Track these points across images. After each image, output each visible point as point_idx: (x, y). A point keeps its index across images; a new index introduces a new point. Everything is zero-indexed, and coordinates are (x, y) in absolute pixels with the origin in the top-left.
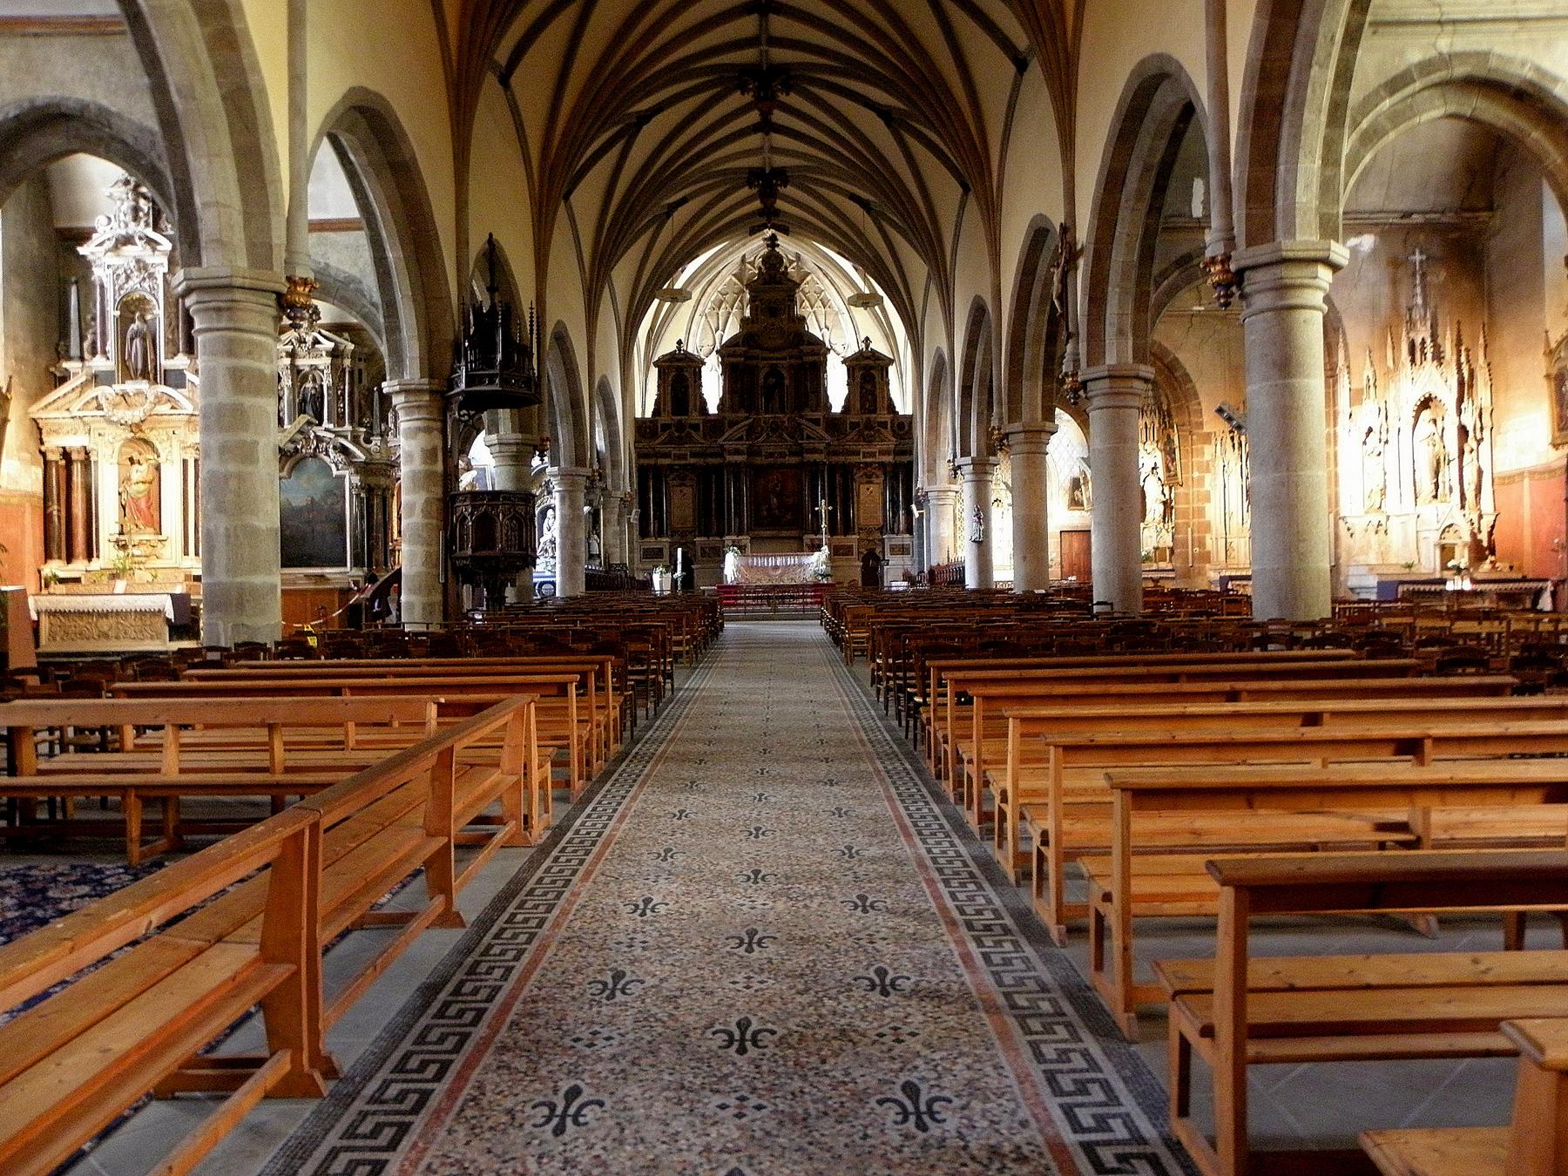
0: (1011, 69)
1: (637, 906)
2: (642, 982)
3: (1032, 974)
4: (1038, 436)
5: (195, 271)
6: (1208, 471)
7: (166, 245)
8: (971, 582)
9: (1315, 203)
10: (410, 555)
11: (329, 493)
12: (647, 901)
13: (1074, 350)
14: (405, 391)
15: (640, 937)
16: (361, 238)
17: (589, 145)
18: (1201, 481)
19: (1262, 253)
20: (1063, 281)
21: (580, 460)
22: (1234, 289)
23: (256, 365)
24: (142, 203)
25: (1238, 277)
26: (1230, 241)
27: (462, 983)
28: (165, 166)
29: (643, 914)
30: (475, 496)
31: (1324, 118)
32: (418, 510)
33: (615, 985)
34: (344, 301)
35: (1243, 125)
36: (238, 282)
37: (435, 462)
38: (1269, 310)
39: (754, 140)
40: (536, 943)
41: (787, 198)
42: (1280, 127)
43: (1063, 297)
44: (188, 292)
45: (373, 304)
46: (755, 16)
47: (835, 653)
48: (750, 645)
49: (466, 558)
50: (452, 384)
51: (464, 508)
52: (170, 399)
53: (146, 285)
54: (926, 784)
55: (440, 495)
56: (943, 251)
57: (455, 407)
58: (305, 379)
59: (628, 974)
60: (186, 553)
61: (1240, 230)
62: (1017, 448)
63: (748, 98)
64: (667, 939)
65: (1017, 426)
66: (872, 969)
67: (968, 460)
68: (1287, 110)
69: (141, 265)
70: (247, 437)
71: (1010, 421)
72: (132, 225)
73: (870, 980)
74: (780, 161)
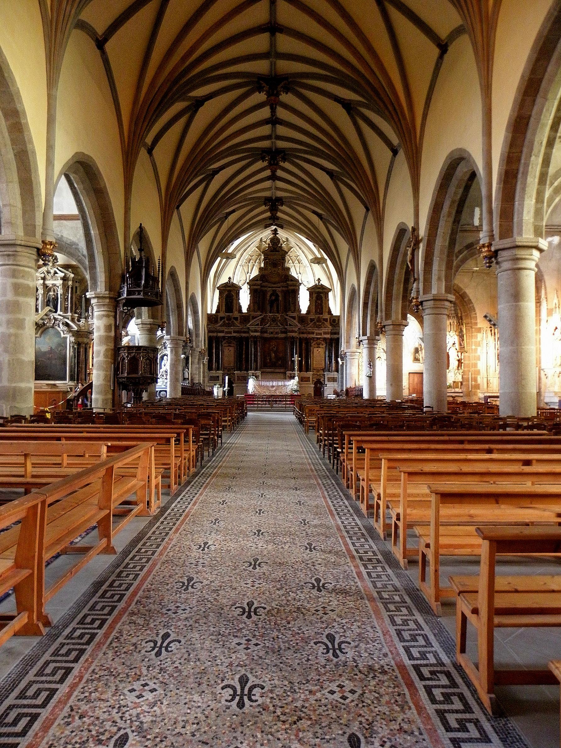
0: (390, 154)
1: (200, 546)
2: (202, 583)
4: (399, 327)
6: (479, 346)
8: (366, 396)
9: (532, 220)
10: (97, 376)
11: (59, 345)
13: (417, 287)
16: (79, 224)
21: (180, 333)
22: (493, 259)
23: (26, 282)
25: (495, 254)
26: (492, 237)
29: (203, 550)
30: (129, 348)
32: (102, 354)
33: (188, 584)
36: (19, 242)
37: (110, 331)
38: (510, 270)
40: (151, 562)
41: (284, 169)
43: (412, 261)
45: (83, 256)
48: (259, 423)
49: (124, 378)
50: (120, 294)
54: (342, 491)
55: (113, 347)
57: (121, 305)
58: (49, 290)
59: (195, 578)
61: (496, 232)
65: (389, 322)
66: (313, 579)
67: (366, 338)
68: (520, 176)
70: (21, 316)
74: (280, 194)
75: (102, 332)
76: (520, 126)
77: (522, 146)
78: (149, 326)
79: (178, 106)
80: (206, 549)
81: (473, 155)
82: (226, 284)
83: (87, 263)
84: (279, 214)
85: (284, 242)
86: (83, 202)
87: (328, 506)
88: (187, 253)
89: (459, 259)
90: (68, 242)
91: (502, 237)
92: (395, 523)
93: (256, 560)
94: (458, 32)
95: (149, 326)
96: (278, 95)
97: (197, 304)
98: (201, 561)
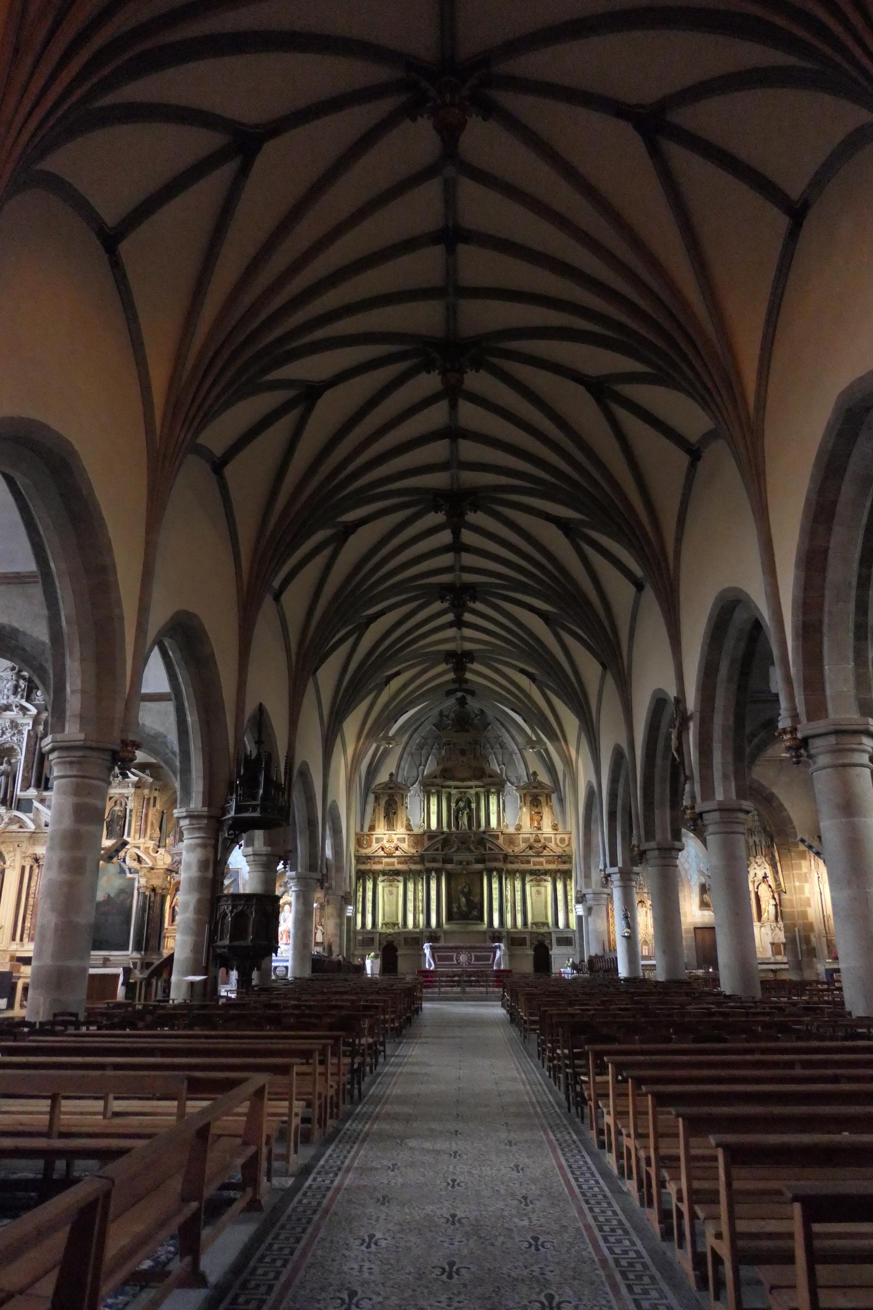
0: (632, 589)
1: (364, 1240)
2: (370, 1299)
3: (665, 1301)
4: (669, 853)
5: (59, 737)
6: (806, 881)
7: (34, 711)
8: (623, 971)
9: (852, 692)
10: (177, 942)
11: (122, 891)
12: (371, 1236)
13: (692, 789)
14: (190, 816)
15: (367, 1265)
16: (169, 707)
17: (333, 637)
18: (802, 889)
19: (820, 726)
20: (679, 738)
21: (312, 867)
22: (802, 751)
24: (22, 683)
25: (805, 742)
26: (795, 717)
27: (237, 1296)
28: (49, 666)
29: (368, 1247)
30: (236, 897)
31: (851, 635)
33: (350, 1301)
34: (153, 751)
35: (796, 637)
38: (829, 767)
39: (446, 559)
40: (289, 1266)
41: (474, 612)
42: (821, 643)
43: (679, 750)
44: (52, 750)
45: (174, 753)
46: (446, 442)
47: (514, 1032)
48: (447, 1024)
49: (224, 947)
50: (225, 811)
51: (226, 907)
52: (19, 820)
53: (15, 738)
54: (590, 1153)
55: (209, 897)
56: (590, 713)
57: (225, 828)
59: (360, 1293)
60: (14, 939)
61: (801, 709)
62: (651, 862)
63: (446, 605)
64: (386, 1267)
65: (653, 845)
66: (543, 1295)
67: (616, 869)
69: (14, 725)
71: (647, 840)
72: (12, 697)
73: (541, 1303)
74: (468, 646)
75: (194, 872)
76: (813, 562)
77: (823, 588)
78: (264, 858)
79: (320, 535)
80: (373, 1245)
81: (753, 597)
82: (386, 784)
83: (178, 764)
84: (469, 676)
85: (476, 716)
86: (179, 676)
87: (561, 1167)
88: (350, 781)
89: (754, 743)
90: (152, 733)
91: (810, 718)
92: (677, 1206)
93: (451, 1264)
94: (710, 436)
95: (264, 858)
96: (462, 515)
97: (339, 818)
98: (367, 1265)
